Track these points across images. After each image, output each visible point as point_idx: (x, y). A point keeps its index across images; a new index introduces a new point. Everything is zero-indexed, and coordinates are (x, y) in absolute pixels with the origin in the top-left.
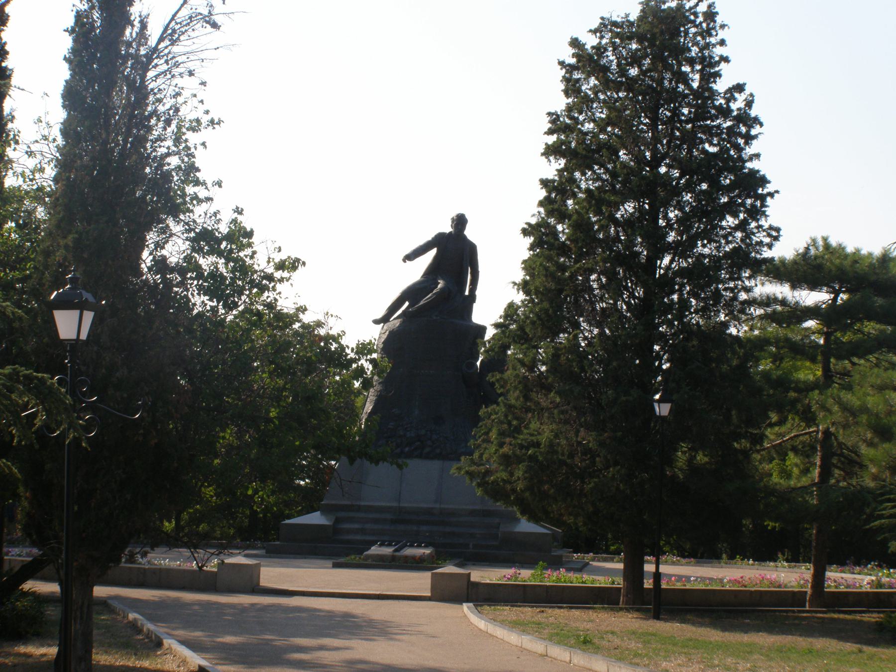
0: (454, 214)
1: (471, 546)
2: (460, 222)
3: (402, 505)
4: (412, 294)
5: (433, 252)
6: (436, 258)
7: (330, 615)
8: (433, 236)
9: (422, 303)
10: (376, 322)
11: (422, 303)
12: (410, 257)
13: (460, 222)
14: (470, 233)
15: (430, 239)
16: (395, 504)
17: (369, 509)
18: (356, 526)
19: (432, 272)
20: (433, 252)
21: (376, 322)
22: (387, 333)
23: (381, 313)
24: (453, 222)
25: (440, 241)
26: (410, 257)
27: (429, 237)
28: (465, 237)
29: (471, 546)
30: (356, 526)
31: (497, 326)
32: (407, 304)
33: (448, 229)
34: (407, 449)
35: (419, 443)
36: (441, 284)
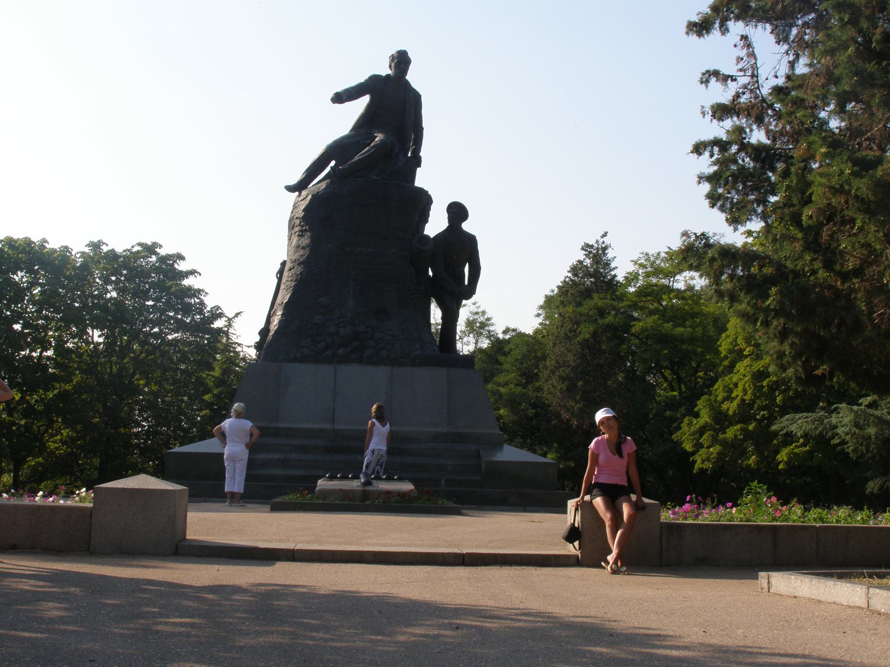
0: (393, 51)
1: (443, 482)
2: (401, 61)
3: (337, 427)
4: (337, 150)
5: (365, 100)
6: (369, 107)
7: (12, 573)
8: (366, 78)
9: (356, 158)
10: (290, 189)
11: (356, 158)
12: (340, 98)
13: (401, 61)
14: (413, 77)
15: (362, 81)
16: (327, 426)
17: (291, 433)
18: (276, 456)
19: (365, 124)
20: (365, 100)
21: (290, 189)
22: (310, 197)
23: (295, 178)
24: (392, 60)
25: (372, 86)
26: (340, 98)
27: (361, 77)
28: (407, 84)
29: (443, 482)
30: (276, 456)
31: (724, 30)
32: (333, 163)
33: (384, 69)
34: (341, 351)
35: (358, 343)
36: (379, 137)
